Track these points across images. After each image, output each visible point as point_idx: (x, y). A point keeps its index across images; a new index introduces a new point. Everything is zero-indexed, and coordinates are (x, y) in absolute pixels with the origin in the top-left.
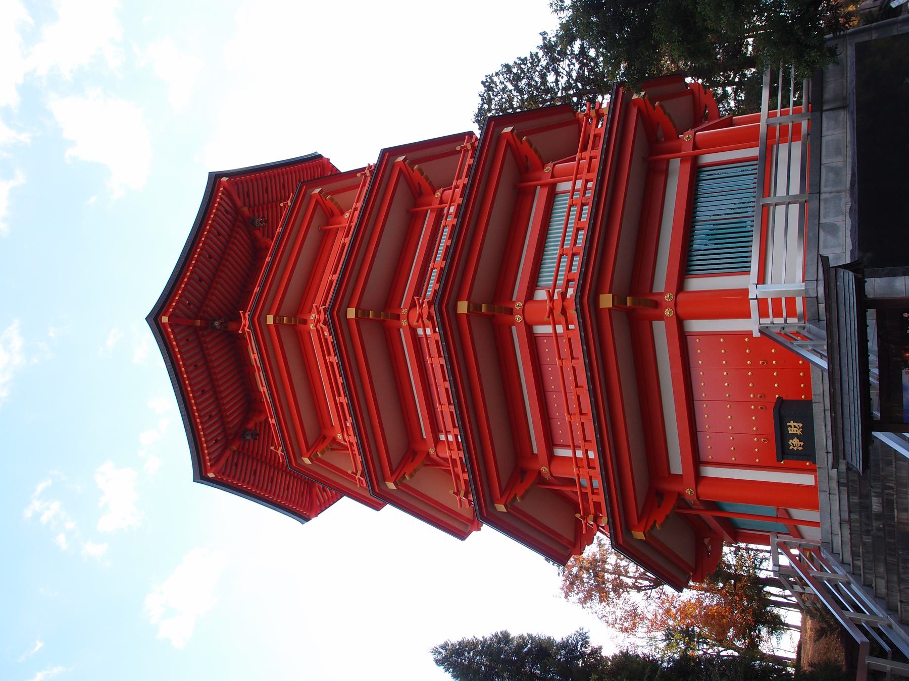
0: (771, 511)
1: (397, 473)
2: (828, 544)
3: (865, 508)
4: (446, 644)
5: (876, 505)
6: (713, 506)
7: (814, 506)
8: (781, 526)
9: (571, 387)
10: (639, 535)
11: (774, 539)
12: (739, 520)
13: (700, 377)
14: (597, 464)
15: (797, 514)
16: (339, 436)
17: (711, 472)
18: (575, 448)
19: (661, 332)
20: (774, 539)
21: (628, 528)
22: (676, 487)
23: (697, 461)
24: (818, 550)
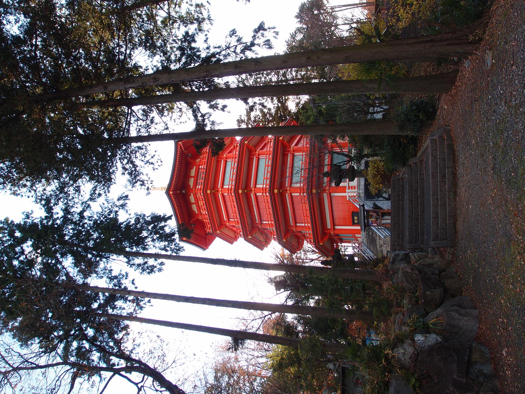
0: (351, 235)
1: (251, 234)
2: (363, 242)
3: (369, 234)
4: (83, 368)
5: (371, 234)
6: (337, 235)
7: (360, 234)
8: (353, 239)
9: (304, 211)
10: (321, 244)
11: (352, 242)
12: (343, 238)
13: (334, 206)
14: (311, 228)
15: (357, 235)
16: (228, 224)
17: (337, 227)
18: (305, 223)
19: (325, 195)
20: (352, 242)
21: (318, 243)
22: (329, 232)
23: (334, 225)
24: (361, 243)
